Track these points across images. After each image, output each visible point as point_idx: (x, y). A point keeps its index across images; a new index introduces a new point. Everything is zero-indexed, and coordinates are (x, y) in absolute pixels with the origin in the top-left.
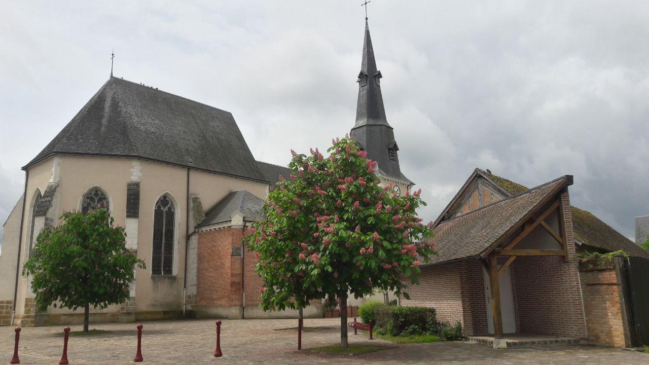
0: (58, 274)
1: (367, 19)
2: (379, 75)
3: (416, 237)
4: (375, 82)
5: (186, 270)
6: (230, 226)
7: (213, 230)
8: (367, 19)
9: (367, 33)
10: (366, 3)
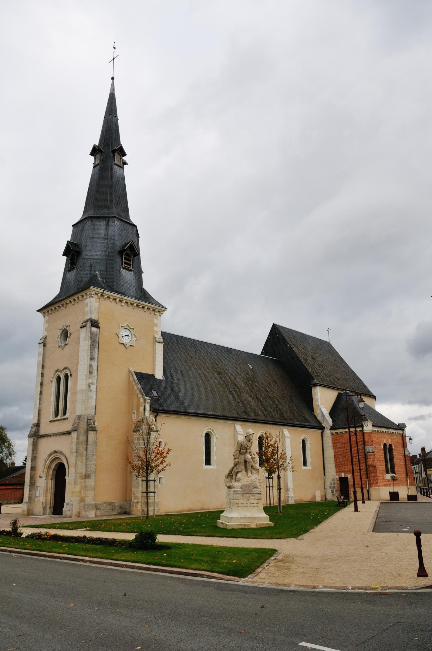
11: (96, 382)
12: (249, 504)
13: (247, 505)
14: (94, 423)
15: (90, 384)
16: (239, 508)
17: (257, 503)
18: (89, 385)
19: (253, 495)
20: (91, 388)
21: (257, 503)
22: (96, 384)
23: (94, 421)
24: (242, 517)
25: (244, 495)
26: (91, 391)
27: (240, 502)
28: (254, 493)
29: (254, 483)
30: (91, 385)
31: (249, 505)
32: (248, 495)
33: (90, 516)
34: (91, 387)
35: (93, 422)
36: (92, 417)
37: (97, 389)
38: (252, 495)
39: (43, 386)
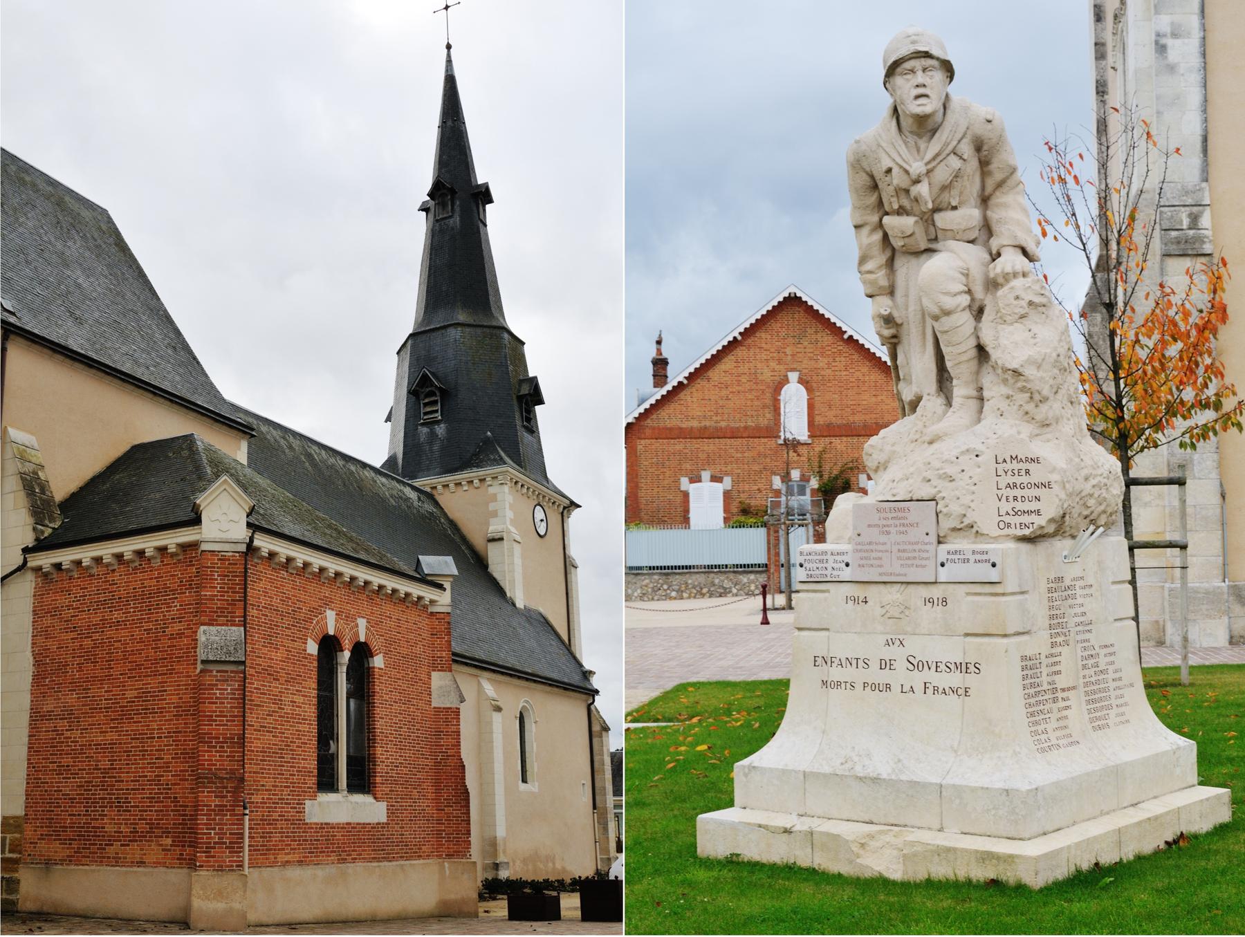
0: (690, 586)
1: (449, 47)
2: (484, 195)
3: (1141, 900)
4: (476, 215)
5: (567, 594)
6: (194, 545)
7: (172, 549)
8: (449, 47)
9: (450, 82)
10: (447, 8)
11: (1195, 21)
12: (901, 665)
13: (884, 677)
14: (1194, 220)
15: (1165, 36)
16: (834, 693)
17: (963, 667)
18: (1157, 43)
19: (936, 592)
20: (1173, 56)
21: (963, 667)
22: (1196, 34)
23: (1195, 209)
24: (816, 775)
25: (872, 592)
26: (1172, 69)
27: (842, 646)
28: (943, 575)
29: (946, 490)
30: (1169, 42)
31: (900, 675)
32: (892, 595)
33: (1205, 645)
34: (1169, 51)
35: (1190, 215)
36: (1187, 193)
37: (1204, 55)
38: (925, 592)
39: (1106, 97)
